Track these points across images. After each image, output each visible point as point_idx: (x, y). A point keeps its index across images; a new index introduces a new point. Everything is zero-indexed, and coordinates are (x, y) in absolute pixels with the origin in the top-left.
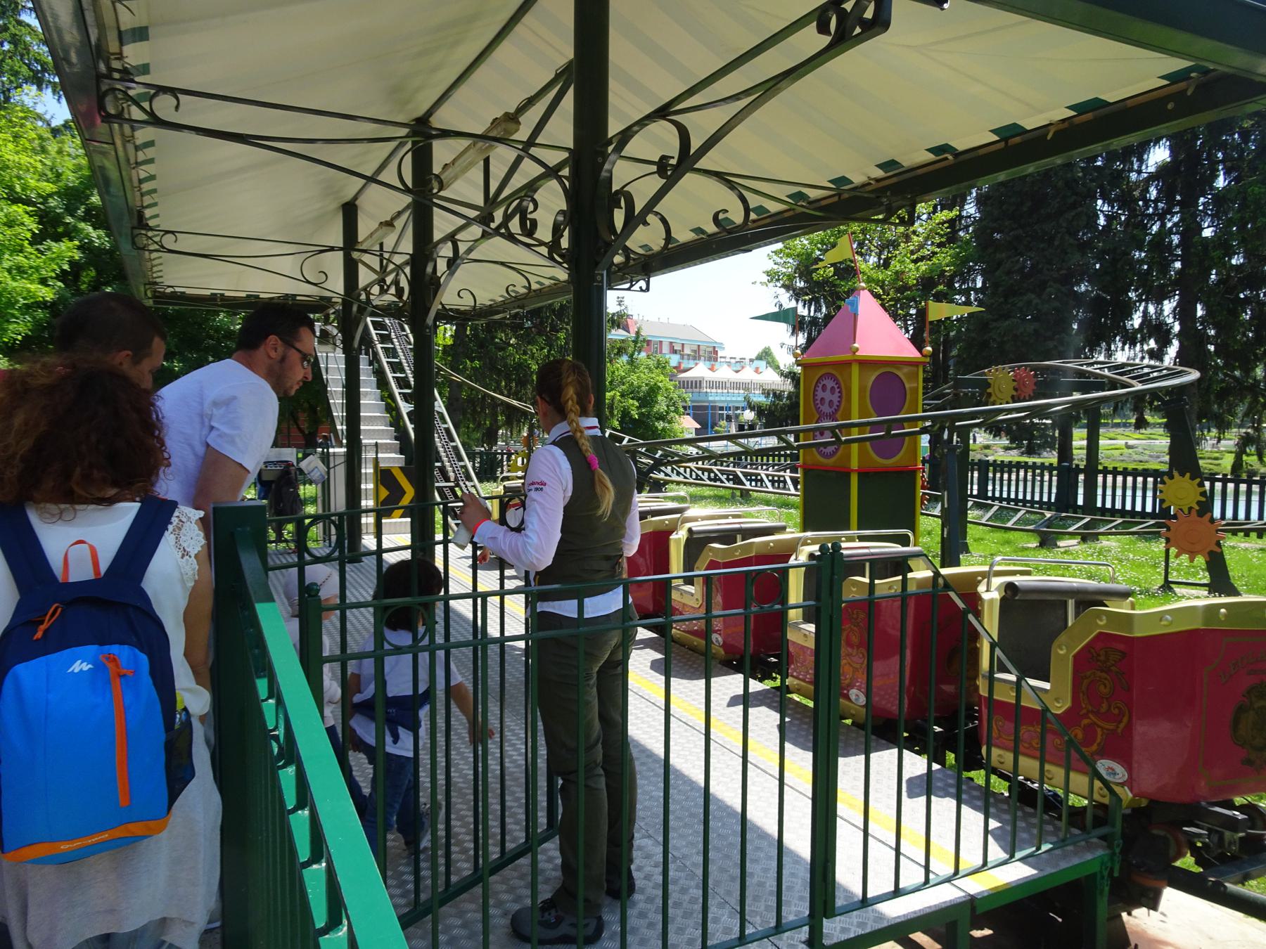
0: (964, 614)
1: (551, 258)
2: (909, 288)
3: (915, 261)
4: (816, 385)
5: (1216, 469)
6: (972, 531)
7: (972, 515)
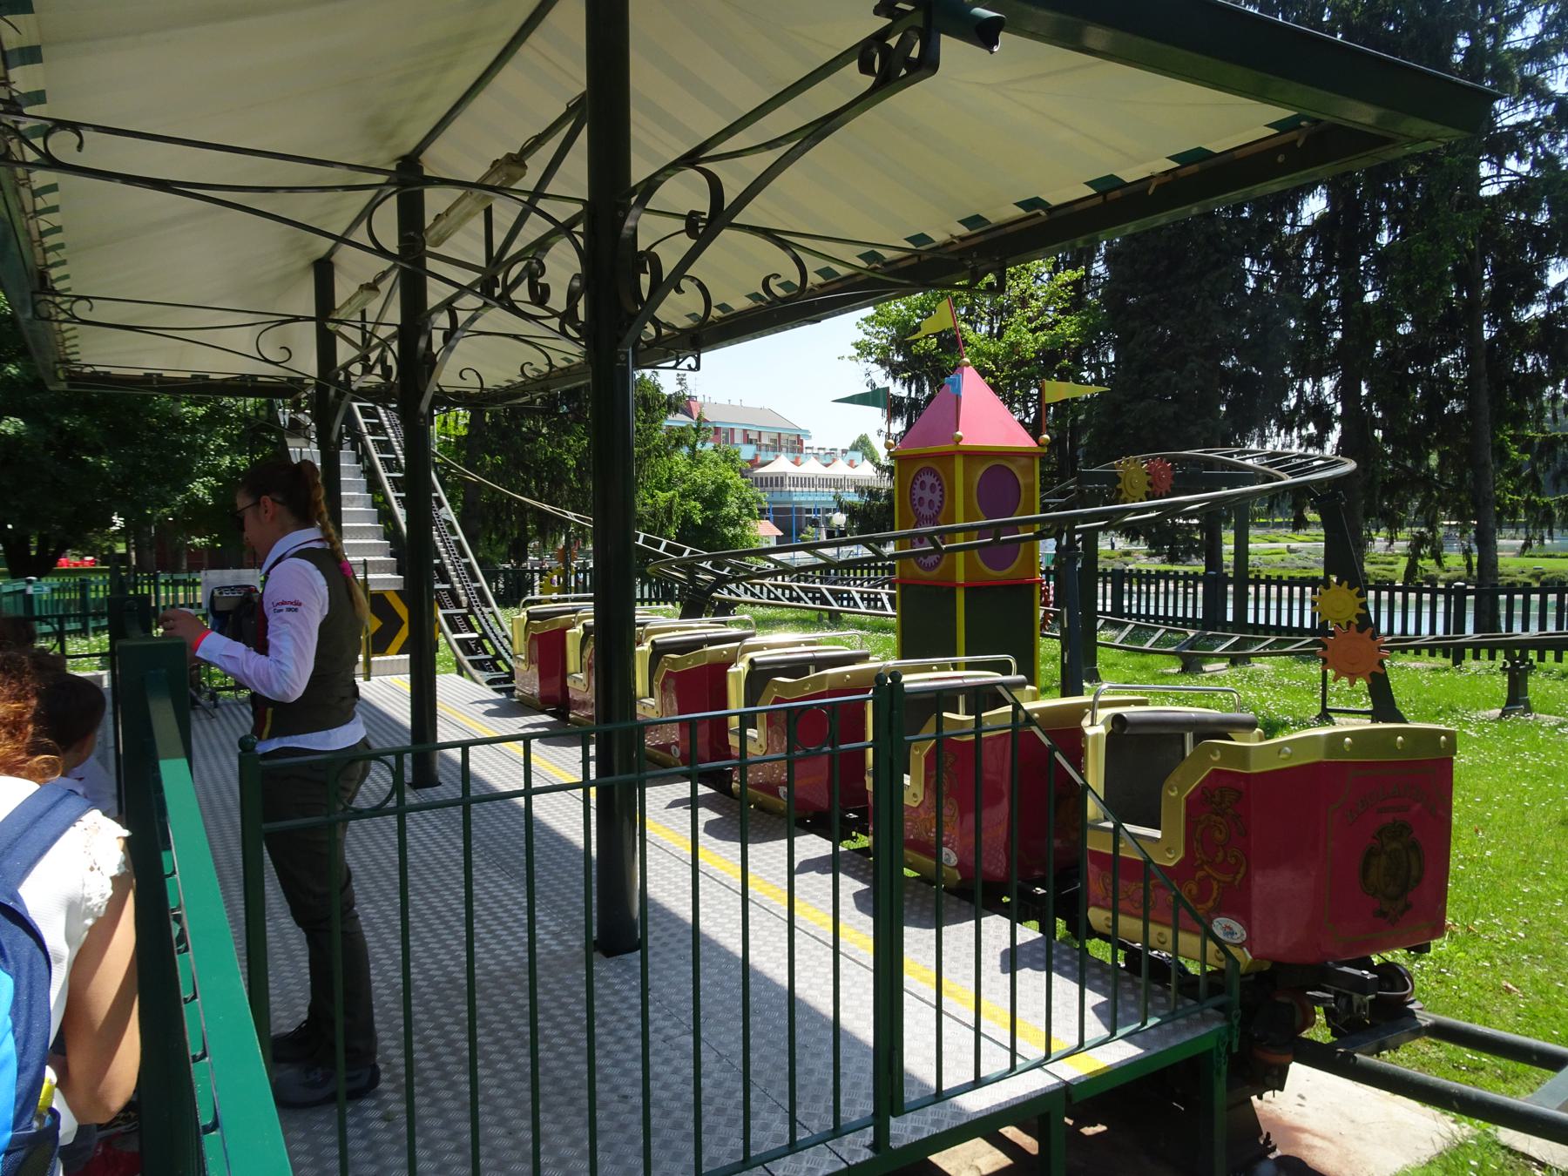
0: (1049, 752)
1: (564, 333)
2: (1027, 363)
3: (1033, 331)
4: (913, 482)
5: (1390, 576)
6: (1103, 655)
7: (1103, 636)
